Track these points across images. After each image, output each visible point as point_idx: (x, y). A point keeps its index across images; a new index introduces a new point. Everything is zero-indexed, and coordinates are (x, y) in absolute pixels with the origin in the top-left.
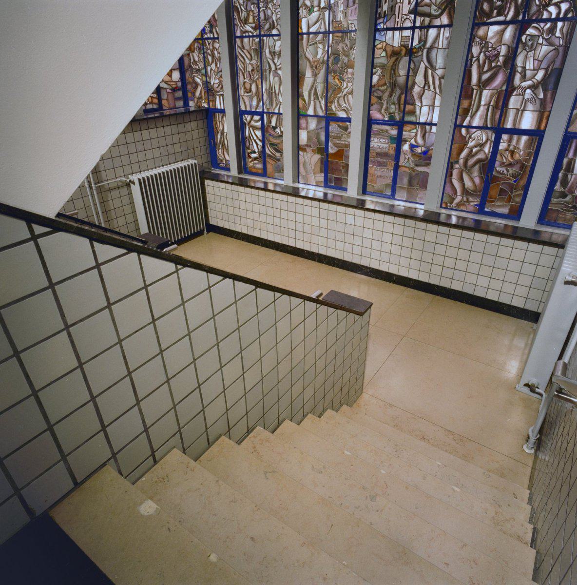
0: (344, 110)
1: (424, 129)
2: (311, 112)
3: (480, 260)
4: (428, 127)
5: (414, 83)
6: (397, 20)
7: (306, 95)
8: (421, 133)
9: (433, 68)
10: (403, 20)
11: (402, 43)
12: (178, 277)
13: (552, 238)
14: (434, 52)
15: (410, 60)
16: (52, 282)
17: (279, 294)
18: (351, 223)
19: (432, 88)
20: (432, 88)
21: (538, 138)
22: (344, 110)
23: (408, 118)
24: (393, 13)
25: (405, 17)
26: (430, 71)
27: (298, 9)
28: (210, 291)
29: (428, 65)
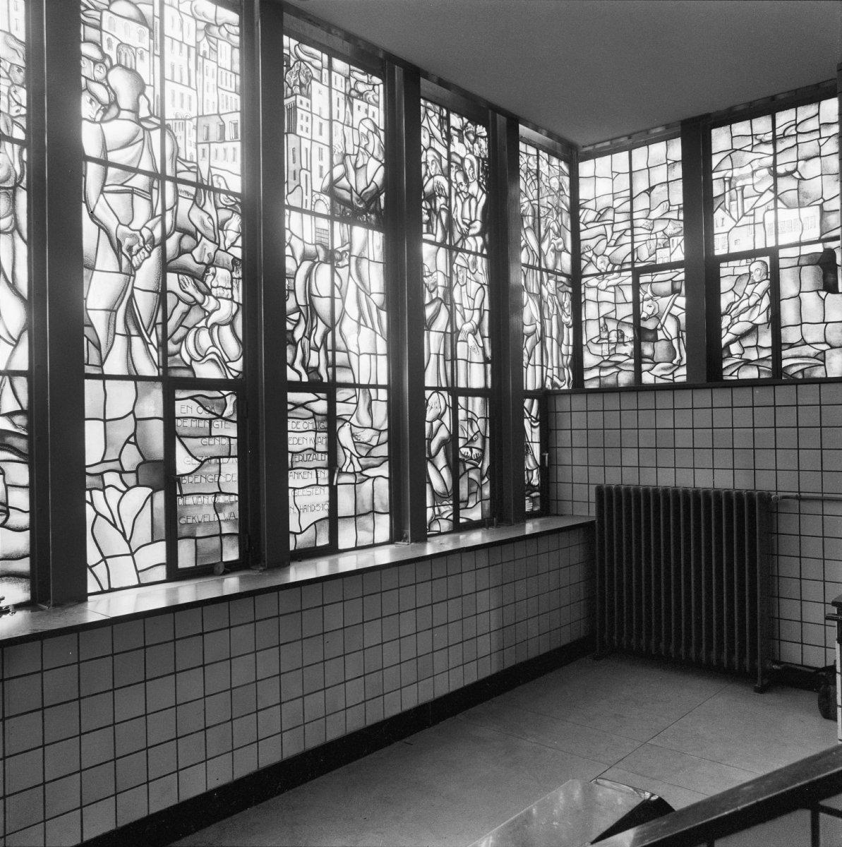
0: (213, 360)
1: (368, 395)
2: (115, 364)
3: (576, 427)
4: (373, 391)
5: (344, 312)
6: (305, 197)
7: (98, 319)
8: (365, 401)
9: (368, 294)
10: (314, 200)
11: (318, 239)
12: (79, 690)
13: (619, 382)
14: (364, 263)
15: (333, 271)
16: (682, 261)
17: (93, 836)
18: (231, 622)
19: (370, 324)
20: (370, 324)
21: (292, 548)
22: (213, 360)
23: (342, 376)
24: (298, 183)
25: (317, 196)
26: (363, 295)
27: (746, 258)
28: (44, 789)
29: (359, 284)
